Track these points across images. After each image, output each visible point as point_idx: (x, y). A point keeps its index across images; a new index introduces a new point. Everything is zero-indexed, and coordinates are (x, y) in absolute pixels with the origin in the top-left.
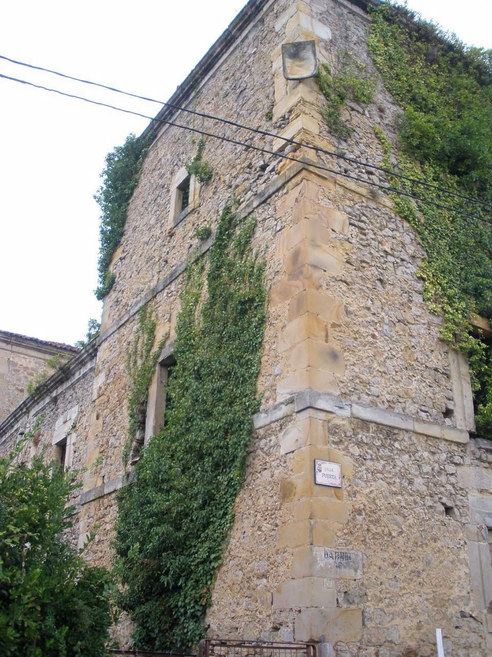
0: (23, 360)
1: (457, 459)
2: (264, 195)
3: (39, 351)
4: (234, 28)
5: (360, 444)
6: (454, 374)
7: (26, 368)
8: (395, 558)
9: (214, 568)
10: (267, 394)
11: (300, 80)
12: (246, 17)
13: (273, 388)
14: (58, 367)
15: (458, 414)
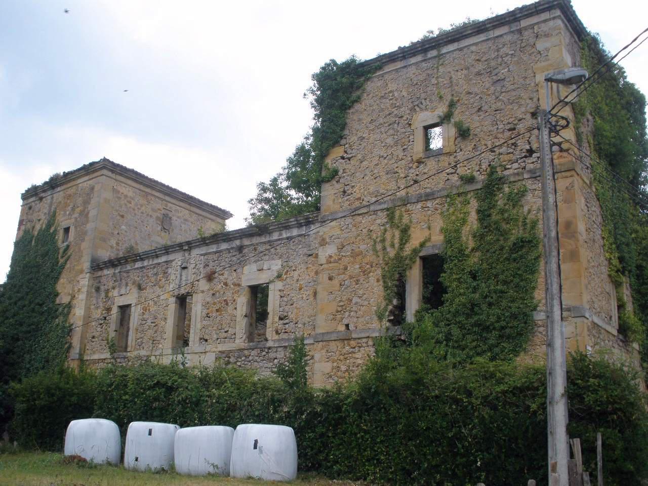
0: (124, 189)
2: (535, 173)
4: (490, 23)
7: (126, 196)
12: (503, 21)
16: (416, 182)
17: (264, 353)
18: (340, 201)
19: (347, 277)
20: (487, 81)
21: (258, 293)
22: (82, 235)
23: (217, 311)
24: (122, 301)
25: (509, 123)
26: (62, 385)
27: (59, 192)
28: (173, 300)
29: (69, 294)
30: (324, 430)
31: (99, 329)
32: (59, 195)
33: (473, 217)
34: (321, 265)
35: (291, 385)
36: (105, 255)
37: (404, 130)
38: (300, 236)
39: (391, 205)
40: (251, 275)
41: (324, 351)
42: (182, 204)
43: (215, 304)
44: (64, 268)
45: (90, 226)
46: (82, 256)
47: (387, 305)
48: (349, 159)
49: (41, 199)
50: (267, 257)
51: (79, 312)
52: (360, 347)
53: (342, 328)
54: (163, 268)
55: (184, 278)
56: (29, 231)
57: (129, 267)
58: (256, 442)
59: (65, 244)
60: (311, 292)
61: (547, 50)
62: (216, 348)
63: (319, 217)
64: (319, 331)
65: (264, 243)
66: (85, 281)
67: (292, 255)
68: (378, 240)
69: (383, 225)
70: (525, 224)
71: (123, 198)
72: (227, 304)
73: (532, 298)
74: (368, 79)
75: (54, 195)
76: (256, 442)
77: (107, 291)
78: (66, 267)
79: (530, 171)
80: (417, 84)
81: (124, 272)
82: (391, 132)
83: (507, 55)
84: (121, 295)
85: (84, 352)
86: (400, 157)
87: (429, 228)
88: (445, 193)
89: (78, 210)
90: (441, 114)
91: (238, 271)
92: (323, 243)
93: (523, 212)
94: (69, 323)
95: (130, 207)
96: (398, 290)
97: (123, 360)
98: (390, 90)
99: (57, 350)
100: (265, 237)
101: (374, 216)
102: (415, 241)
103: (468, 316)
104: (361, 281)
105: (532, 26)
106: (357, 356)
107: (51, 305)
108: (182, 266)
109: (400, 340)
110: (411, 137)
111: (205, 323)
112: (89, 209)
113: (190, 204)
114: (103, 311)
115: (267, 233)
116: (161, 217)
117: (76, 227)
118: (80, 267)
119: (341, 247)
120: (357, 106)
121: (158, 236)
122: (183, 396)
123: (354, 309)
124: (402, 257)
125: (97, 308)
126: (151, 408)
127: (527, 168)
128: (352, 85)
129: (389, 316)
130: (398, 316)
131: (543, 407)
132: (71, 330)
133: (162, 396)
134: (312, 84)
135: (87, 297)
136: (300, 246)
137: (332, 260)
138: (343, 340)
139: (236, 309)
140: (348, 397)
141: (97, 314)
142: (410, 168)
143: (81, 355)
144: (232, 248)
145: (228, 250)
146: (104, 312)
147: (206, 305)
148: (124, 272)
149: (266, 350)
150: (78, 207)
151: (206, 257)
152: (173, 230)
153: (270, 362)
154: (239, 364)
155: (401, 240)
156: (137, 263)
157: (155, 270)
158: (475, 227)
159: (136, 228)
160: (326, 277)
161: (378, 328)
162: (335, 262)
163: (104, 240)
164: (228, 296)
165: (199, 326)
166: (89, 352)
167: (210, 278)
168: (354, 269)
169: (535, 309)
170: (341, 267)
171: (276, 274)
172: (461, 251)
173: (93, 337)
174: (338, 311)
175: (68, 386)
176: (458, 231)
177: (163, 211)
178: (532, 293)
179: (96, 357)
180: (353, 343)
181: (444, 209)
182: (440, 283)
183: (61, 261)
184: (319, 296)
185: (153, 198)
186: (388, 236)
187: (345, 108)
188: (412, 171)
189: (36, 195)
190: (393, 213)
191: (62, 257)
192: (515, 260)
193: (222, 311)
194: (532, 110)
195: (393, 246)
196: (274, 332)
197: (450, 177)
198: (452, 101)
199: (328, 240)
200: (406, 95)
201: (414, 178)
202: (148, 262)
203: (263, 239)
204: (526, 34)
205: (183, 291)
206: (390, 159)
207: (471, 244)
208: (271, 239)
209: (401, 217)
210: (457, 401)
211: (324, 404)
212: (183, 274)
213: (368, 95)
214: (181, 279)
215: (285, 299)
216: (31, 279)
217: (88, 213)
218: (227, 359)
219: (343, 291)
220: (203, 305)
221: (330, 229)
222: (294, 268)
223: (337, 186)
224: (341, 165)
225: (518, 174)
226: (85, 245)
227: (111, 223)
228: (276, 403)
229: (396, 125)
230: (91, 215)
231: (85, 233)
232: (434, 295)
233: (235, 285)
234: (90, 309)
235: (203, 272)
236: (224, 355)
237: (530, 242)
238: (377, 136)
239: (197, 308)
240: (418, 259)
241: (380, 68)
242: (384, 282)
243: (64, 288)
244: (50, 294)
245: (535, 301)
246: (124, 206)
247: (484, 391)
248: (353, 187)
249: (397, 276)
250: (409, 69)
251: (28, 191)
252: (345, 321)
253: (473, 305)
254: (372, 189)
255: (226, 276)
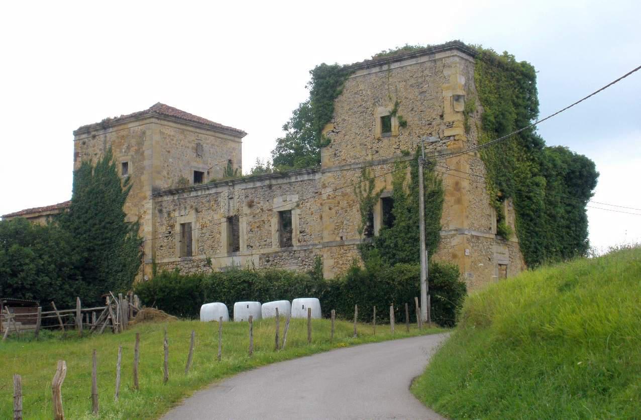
0: (167, 130)
1: (492, 244)
3: (175, 122)
5: (473, 242)
6: (492, 215)
7: (169, 136)
8: (479, 274)
9: (537, 300)
10: (445, 225)
11: (458, 112)
13: (448, 224)
14: (260, 165)
15: (493, 229)
16: (377, 152)
17: (292, 254)
18: (333, 160)
19: (340, 209)
20: (416, 91)
21: (285, 219)
22: (140, 170)
23: (258, 227)
24: (183, 220)
25: (428, 120)
26: (168, 285)
27: (111, 132)
28: (225, 220)
29: (136, 215)
30: (332, 299)
31: (165, 241)
32: (112, 135)
33: (409, 176)
34: (324, 200)
35: (315, 279)
36: (164, 185)
37: (369, 118)
38: (308, 180)
39: (363, 166)
40: (279, 203)
41: (329, 253)
42: (208, 133)
43: (255, 222)
44: (127, 195)
45: (146, 163)
46: (143, 186)
47: (364, 225)
48: (337, 133)
49: (94, 137)
50: (289, 193)
51: (146, 229)
52: (350, 250)
53: (338, 239)
54: (214, 197)
55: (231, 205)
56: (87, 163)
57: (185, 195)
58: (303, 306)
59: (126, 176)
60: (318, 216)
61: (449, 76)
62: (260, 251)
63: (321, 169)
64: (325, 240)
65: (286, 183)
66: (149, 205)
67: (305, 192)
68: (357, 186)
69: (360, 177)
70: (435, 182)
71: (168, 138)
72: (264, 223)
73: (439, 223)
74: (346, 79)
75: (107, 134)
76: (303, 306)
77: (169, 214)
78: (130, 194)
79: (438, 151)
80: (376, 87)
81: (182, 199)
82: (362, 118)
83: (428, 76)
84: (182, 216)
85: (155, 258)
86: (368, 135)
87: (385, 181)
88: (393, 160)
89: (133, 149)
90: (391, 110)
91: (269, 201)
92: (324, 186)
93: (434, 175)
94: (139, 237)
95: (173, 143)
96: (369, 217)
97: (189, 262)
98: (360, 89)
99: (132, 257)
100: (287, 179)
101: (354, 172)
102: (379, 186)
103: (406, 234)
104: (348, 211)
105: (441, 59)
106: (348, 255)
107: (121, 224)
108: (230, 197)
109: (372, 246)
110: (374, 122)
111: (250, 235)
112: (144, 149)
113: (215, 132)
114: (168, 227)
115: (287, 177)
116: (195, 146)
117: (133, 163)
118: (143, 195)
119: (335, 190)
120: (340, 98)
121: (195, 161)
122: (260, 287)
123: (345, 227)
124: (371, 198)
125: (162, 225)
126: (241, 295)
127: (437, 149)
128: (337, 82)
129: (365, 232)
130: (370, 232)
131: (419, 285)
132: (142, 242)
133: (247, 288)
134: (309, 78)
135: (152, 217)
136: (310, 187)
137: (330, 197)
138: (340, 246)
139: (270, 226)
140: (343, 282)
141: (163, 229)
142: (374, 143)
143: (153, 260)
144: (264, 186)
145: (262, 187)
146: (168, 228)
147: (249, 223)
148: (182, 199)
149: (293, 252)
150: (133, 147)
151: (246, 191)
152: (204, 155)
153: (296, 259)
154: (276, 261)
155: (370, 187)
156: (192, 193)
157: (208, 198)
158: (410, 181)
159: (179, 159)
160: (327, 208)
161: (359, 239)
162: (333, 198)
163: (159, 173)
164: (265, 217)
165: (246, 237)
166: (159, 257)
167: (250, 205)
168: (344, 204)
169: (440, 229)
170: (337, 202)
171: (295, 204)
172: (402, 196)
173: (161, 246)
174: (335, 229)
175: (171, 285)
176: (401, 184)
177: (197, 142)
178: (439, 221)
179: (166, 260)
180: (345, 248)
181: (393, 170)
182: (392, 214)
183: (124, 189)
184: (324, 220)
185: (188, 133)
186: (362, 184)
187: (332, 98)
188: (375, 145)
189: (89, 132)
190: (364, 170)
191: (125, 186)
192: (430, 202)
193: (261, 227)
194: (440, 114)
195: (365, 190)
196: (297, 241)
197: (396, 150)
198: (397, 101)
199: (327, 185)
200: (370, 94)
201: (376, 149)
202: (202, 192)
203: (285, 181)
204: (438, 63)
205: (232, 214)
206: (362, 136)
207: (408, 192)
208: (290, 181)
209: (369, 173)
210: (388, 284)
211: (332, 287)
212: (230, 202)
213: (347, 90)
214: (229, 206)
215: (303, 220)
216: (98, 203)
217: (143, 152)
218: (267, 258)
219: (338, 217)
220: (247, 224)
221: (328, 177)
222: (307, 201)
223: (331, 150)
224: (332, 136)
225: (432, 152)
226: (144, 177)
227: (162, 159)
228: (309, 288)
229: (364, 113)
230: (146, 153)
231: (143, 168)
232: (389, 221)
233: (269, 210)
234: (155, 225)
235: (246, 201)
236: (265, 256)
237: (438, 193)
238: (354, 119)
239: (243, 226)
240: (379, 199)
241: (354, 72)
242: (361, 212)
243: (130, 211)
244: (119, 215)
245: (440, 225)
246: (169, 144)
247: (399, 279)
248: (340, 152)
249: (368, 209)
250: (371, 76)
251: (81, 129)
252: (340, 235)
253: (409, 227)
254: (352, 154)
255: (262, 204)
